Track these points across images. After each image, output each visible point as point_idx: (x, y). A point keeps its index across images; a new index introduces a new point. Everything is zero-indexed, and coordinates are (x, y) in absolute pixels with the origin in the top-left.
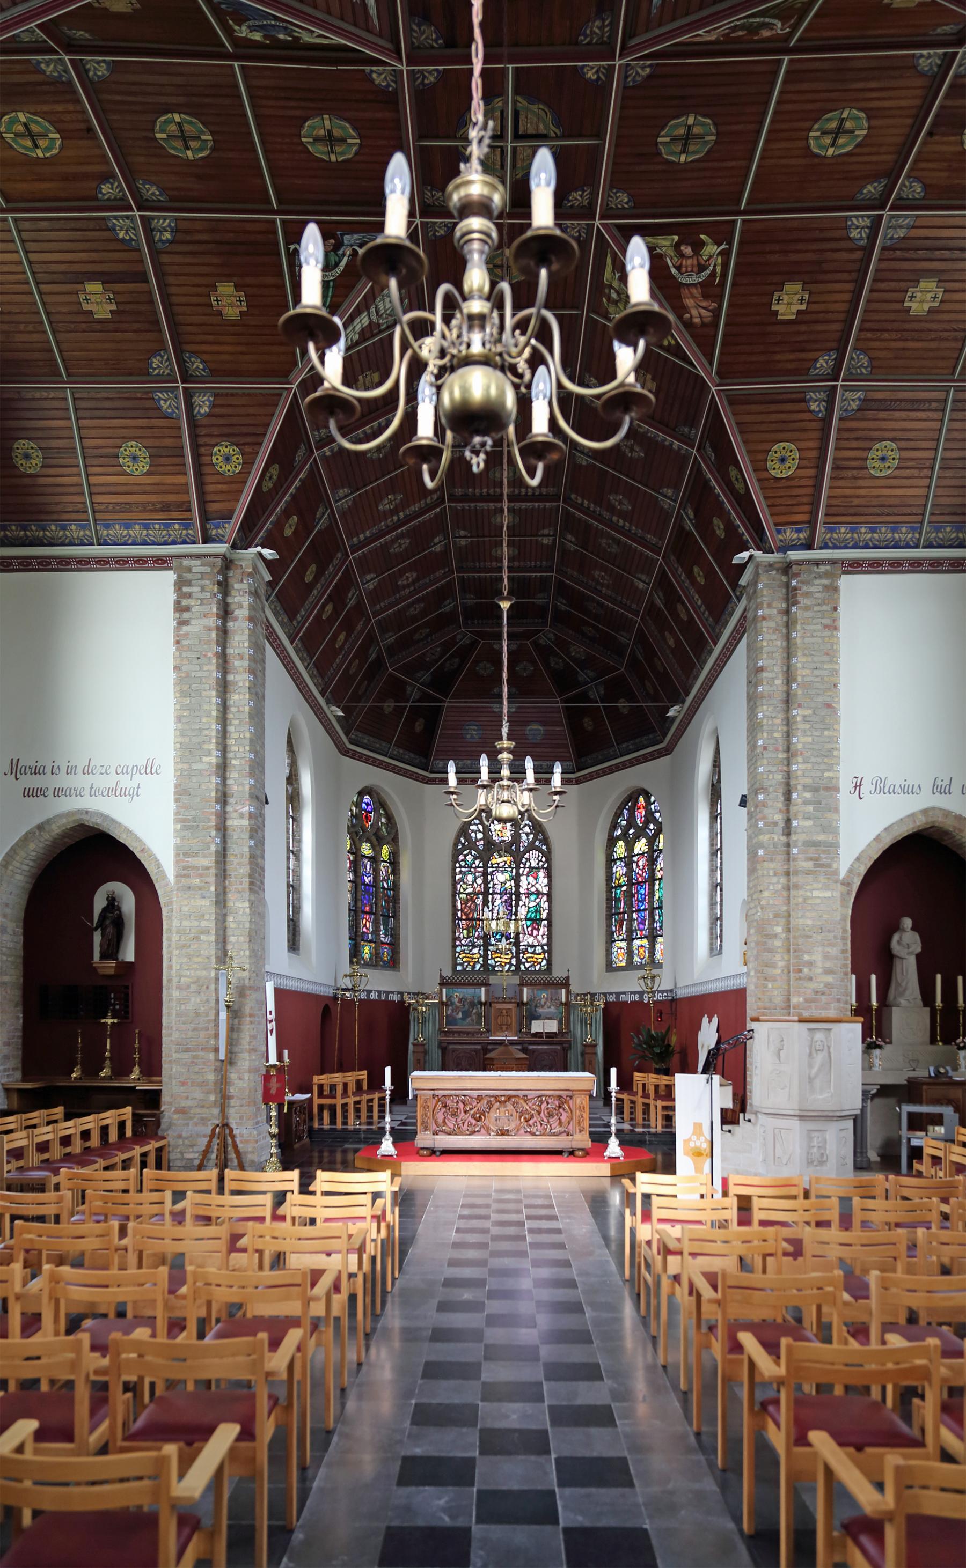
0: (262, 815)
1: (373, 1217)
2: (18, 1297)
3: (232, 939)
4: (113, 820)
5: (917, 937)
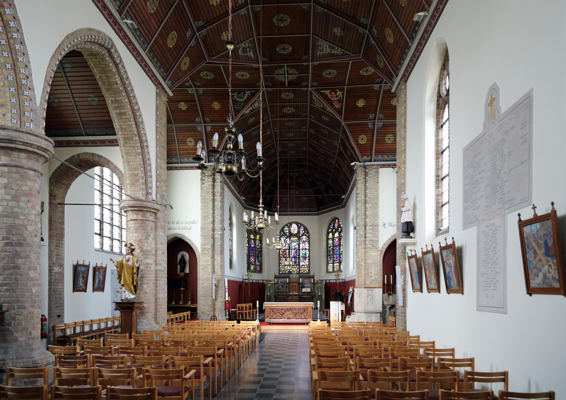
0: (223, 234)
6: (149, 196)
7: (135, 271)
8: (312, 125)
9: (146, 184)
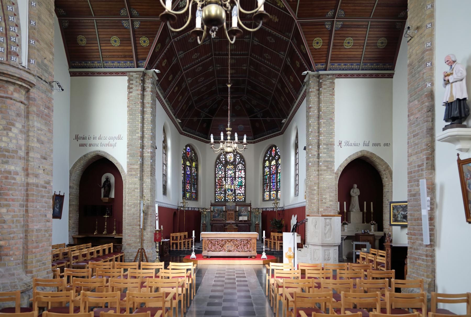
0: (155, 153)
1: (187, 276)
2: (73, 301)
3: (145, 191)
4: (108, 154)
5: (358, 190)
6: (13, 58)
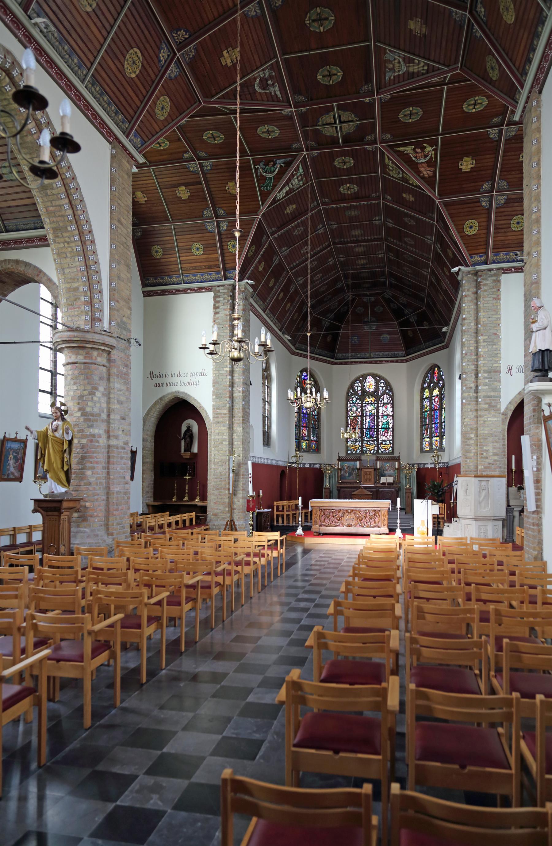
0: (248, 391)
3: (235, 443)
6: (97, 324)
7: (66, 446)
8: (390, 212)
9: (91, 303)
